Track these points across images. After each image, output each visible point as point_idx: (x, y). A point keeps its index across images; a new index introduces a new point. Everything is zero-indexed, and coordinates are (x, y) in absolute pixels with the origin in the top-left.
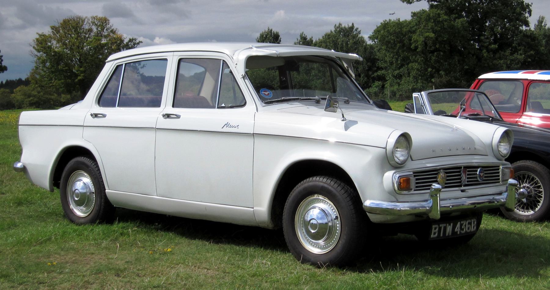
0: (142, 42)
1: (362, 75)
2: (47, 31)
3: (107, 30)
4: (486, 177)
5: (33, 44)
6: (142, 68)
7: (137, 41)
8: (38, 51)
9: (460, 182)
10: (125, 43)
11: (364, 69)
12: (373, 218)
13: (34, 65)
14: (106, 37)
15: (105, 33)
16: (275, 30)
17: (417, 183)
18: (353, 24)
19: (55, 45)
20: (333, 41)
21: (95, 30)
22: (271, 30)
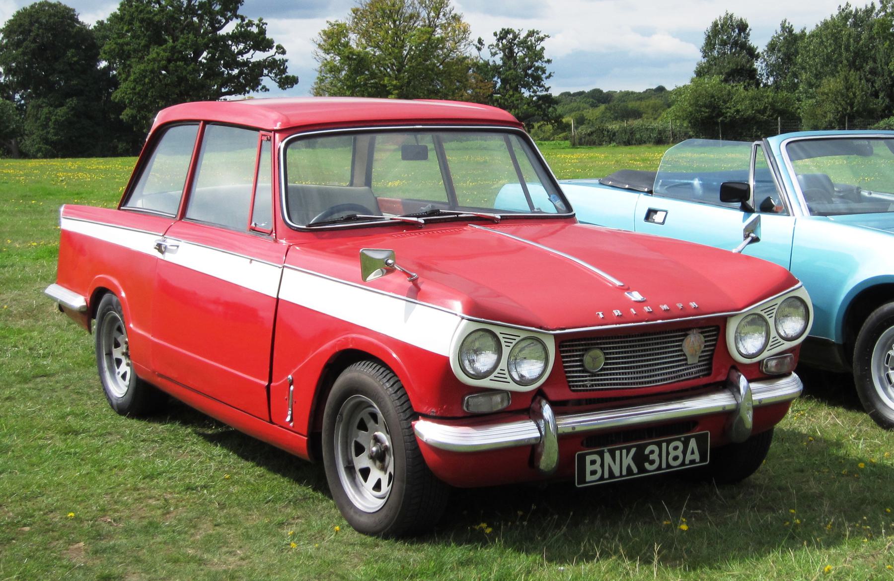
0: (548, 36)
1: (881, 95)
2: (344, 17)
3: (444, 15)
4: (592, 385)
5: (320, 40)
6: (547, 78)
7: (541, 35)
8: (327, 51)
9: (686, 364)
10: (522, 38)
11: (885, 83)
12: (430, 458)
13: (317, 74)
14: (442, 26)
15: (442, 20)
16: (737, 16)
17: (706, 341)
18: (872, 4)
19: (354, 40)
20: (833, 35)
21: (424, 14)
22: (731, 17)
